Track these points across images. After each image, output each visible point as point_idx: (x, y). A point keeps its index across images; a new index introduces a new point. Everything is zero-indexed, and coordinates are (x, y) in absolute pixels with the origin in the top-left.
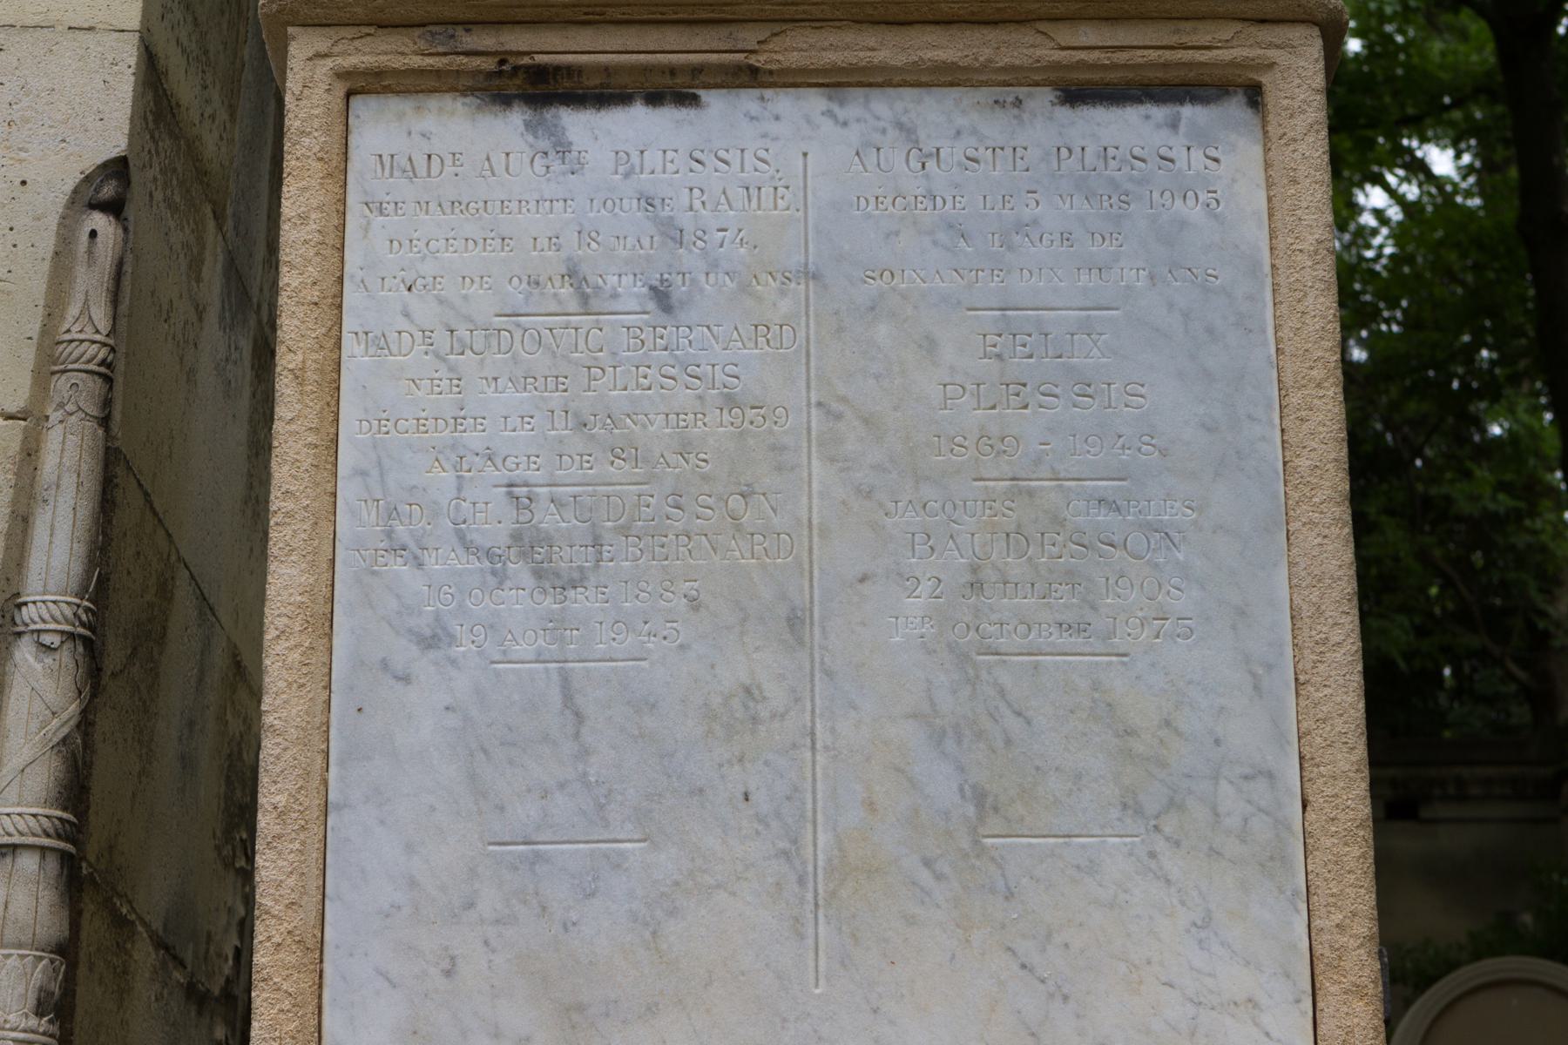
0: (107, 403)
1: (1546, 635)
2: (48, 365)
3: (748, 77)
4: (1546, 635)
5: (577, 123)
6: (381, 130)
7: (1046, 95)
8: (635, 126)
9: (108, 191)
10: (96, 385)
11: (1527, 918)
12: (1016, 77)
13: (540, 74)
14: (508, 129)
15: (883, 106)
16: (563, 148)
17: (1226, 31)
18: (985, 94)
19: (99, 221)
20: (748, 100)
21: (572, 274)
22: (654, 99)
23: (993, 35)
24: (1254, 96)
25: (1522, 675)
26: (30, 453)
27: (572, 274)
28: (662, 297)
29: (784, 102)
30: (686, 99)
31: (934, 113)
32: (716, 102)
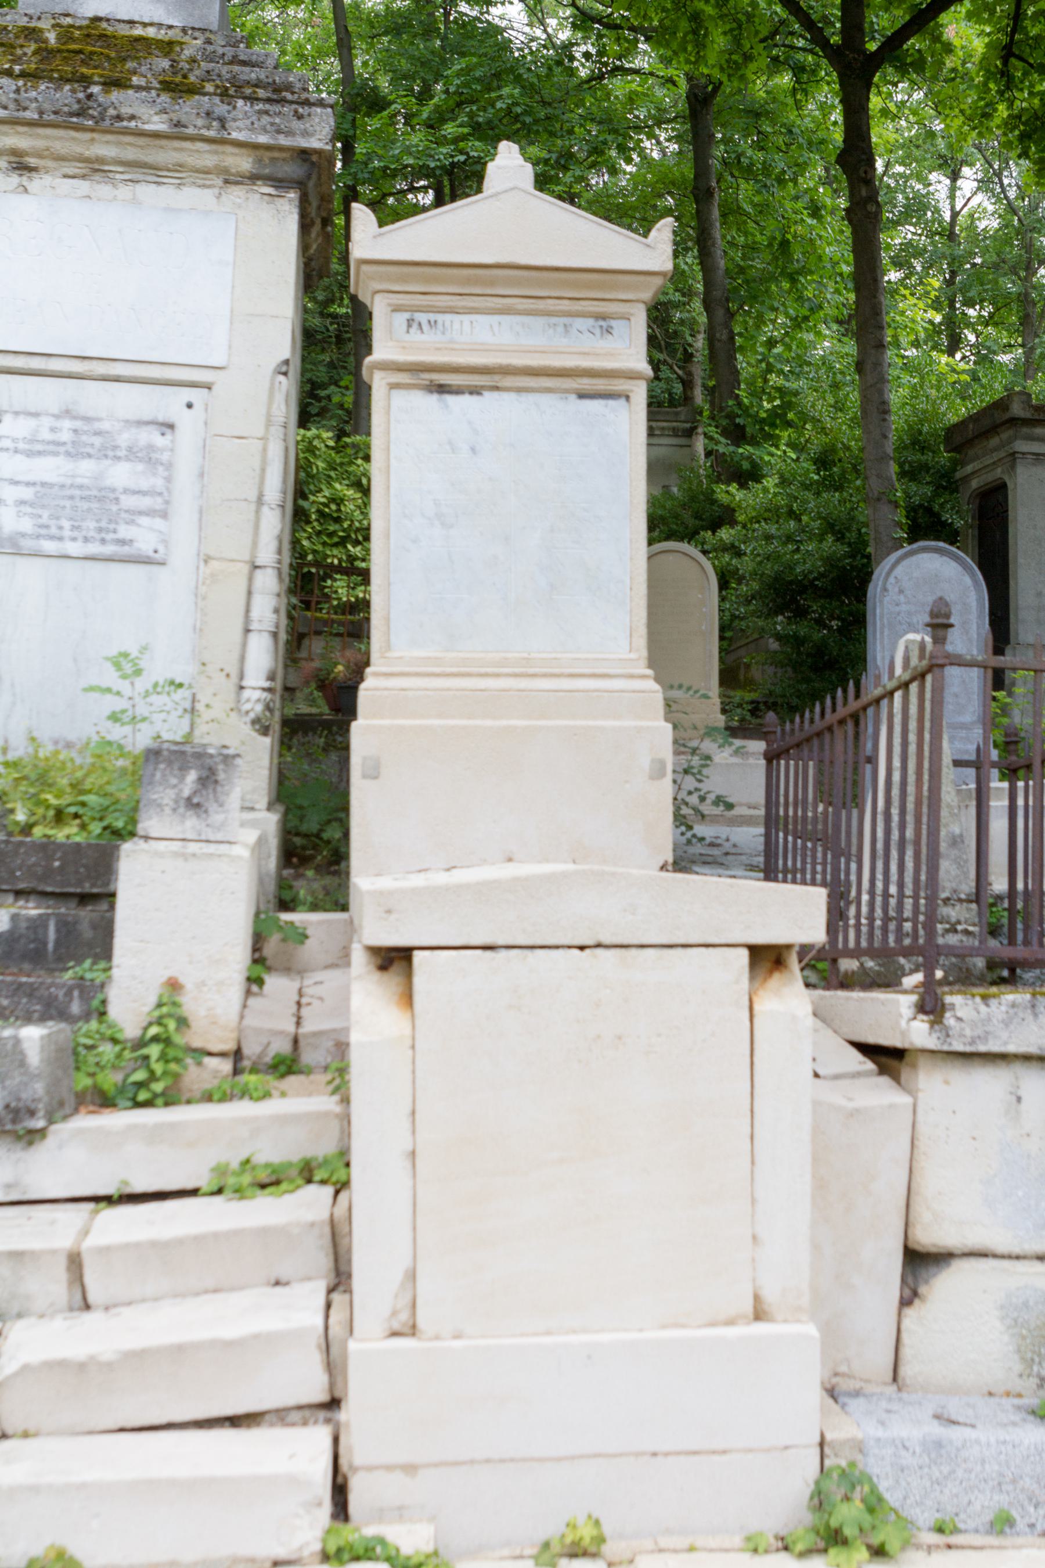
0: (285, 435)
1: (692, 355)
2: (269, 423)
3: (497, 388)
4: (692, 355)
5: (450, 399)
6: (400, 398)
7: (573, 397)
8: (466, 399)
9: (284, 369)
10: (282, 430)
11: (675, 490)
12: (567, 391)
13: (441, 386)
14: (433, 400)
15: (532, 398)
16: (447, 406)
17: (622, 381)
18: (558, 395)
19: (282, 378)
20: (496, 394)
21: (450, 443)
22: (471, 393)
23: (560, 379)
24: (628, 398)
25: (680, 372)
26: (265, 450)
27: (450, 443)
28: (473, 450)
29: (505, 396)
30: (479, 393)
31: (546, 400)
32: (487, 394)
